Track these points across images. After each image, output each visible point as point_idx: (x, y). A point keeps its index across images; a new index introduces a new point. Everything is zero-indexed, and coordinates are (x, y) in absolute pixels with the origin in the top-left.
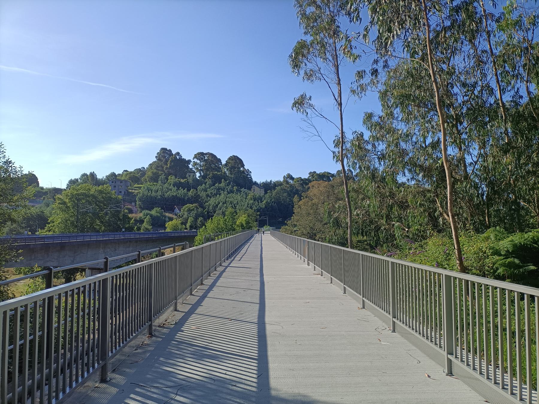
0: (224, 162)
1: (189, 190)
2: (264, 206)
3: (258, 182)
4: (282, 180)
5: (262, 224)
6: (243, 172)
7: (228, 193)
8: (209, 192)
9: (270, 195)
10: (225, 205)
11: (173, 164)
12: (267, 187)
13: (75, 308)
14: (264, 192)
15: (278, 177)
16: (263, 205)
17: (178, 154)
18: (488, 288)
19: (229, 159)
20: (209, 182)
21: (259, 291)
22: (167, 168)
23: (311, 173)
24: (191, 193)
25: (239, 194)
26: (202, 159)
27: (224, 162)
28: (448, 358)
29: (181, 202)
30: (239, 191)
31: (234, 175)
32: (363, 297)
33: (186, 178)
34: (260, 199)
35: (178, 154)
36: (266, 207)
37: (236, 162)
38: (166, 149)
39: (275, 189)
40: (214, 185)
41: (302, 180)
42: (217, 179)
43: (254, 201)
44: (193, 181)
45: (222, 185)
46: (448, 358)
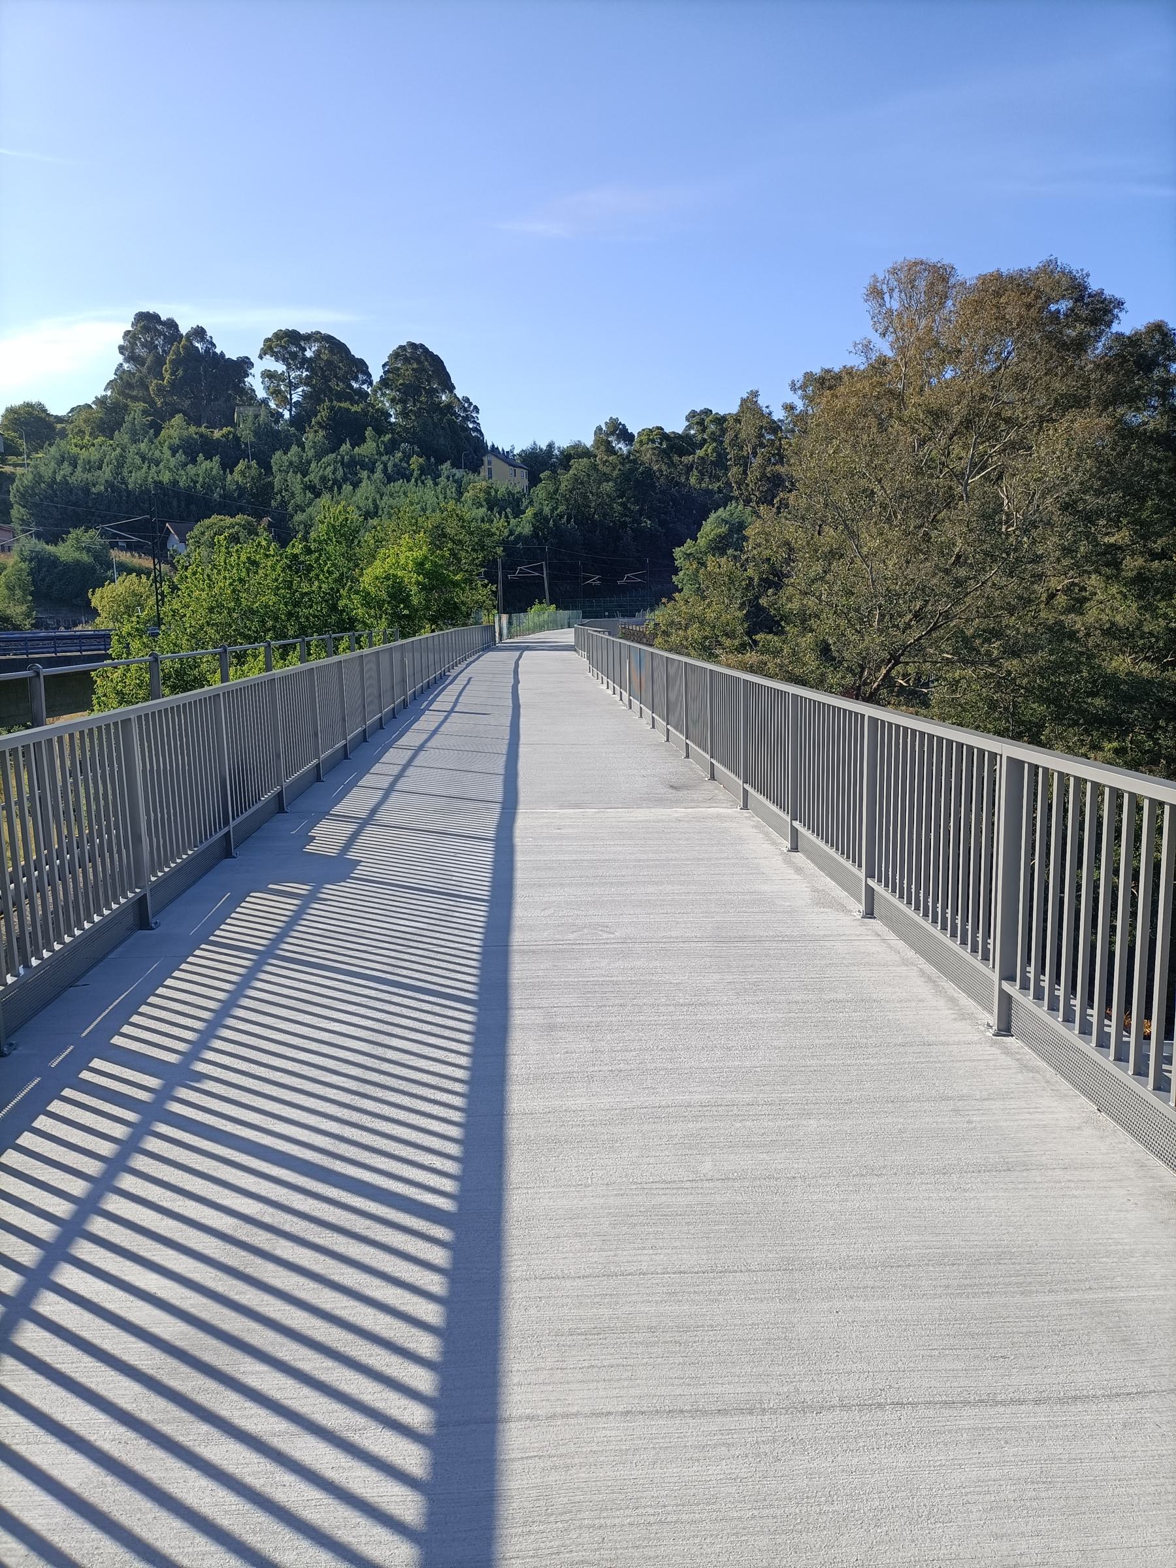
0: (377, 373)
1: (228, 465)
2: (527, 529)
3: (503, 445)
4: (589, 441)
5: (516, 600)
6: (449, 406)
7: (390, 479)
8: (314, 477)
9: (551, 488)
10: (375, 521)
11: (180, 372)
12: (537, 463)
13: (26, 795)
14: (526, 482)
15: (570, 428)
16: (524, 525)
17: (200, 333)
18: (1102, 794)
19: (396, 355)
20: (313, 437)
21: (491, 844)
22: (160, 389)
23: (693, 414)
24: (241, 474)
25: (430, 483)
26: (294, 356)
27: (377, 373)
28: (1001, 991)
29: (188, 506)
30: (430, 472)
31: (415, 417)
32: (870, 874)
33: (231, 423)
34: (512, 504)
35: (200, 333)
36: (535, 534)
37: (420, 369)
38: (155, 318)
39: (567, 468)
40: (335, 449)
41: (665, 436)
42: (346, 428)
43: (490, 509)
44: (256, 433)
45: (368, 448)
46: (1001, 991)
